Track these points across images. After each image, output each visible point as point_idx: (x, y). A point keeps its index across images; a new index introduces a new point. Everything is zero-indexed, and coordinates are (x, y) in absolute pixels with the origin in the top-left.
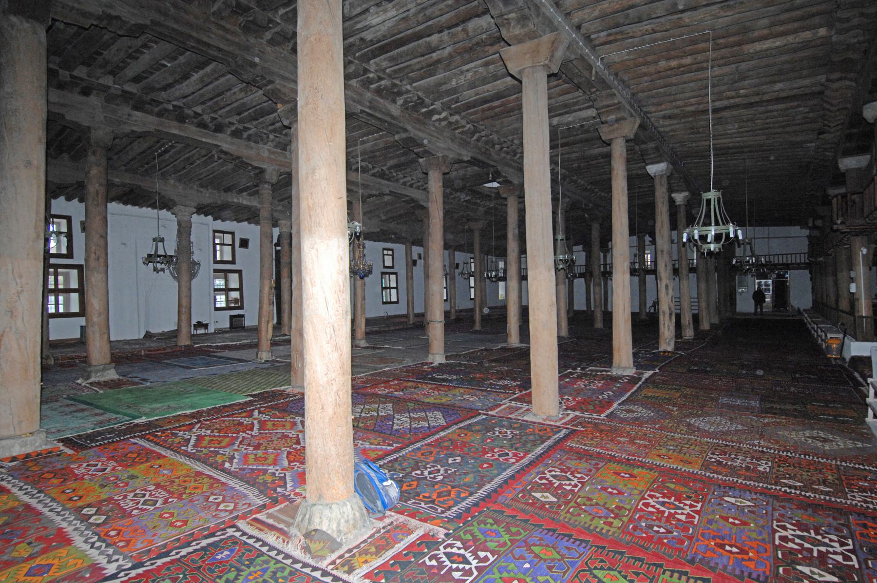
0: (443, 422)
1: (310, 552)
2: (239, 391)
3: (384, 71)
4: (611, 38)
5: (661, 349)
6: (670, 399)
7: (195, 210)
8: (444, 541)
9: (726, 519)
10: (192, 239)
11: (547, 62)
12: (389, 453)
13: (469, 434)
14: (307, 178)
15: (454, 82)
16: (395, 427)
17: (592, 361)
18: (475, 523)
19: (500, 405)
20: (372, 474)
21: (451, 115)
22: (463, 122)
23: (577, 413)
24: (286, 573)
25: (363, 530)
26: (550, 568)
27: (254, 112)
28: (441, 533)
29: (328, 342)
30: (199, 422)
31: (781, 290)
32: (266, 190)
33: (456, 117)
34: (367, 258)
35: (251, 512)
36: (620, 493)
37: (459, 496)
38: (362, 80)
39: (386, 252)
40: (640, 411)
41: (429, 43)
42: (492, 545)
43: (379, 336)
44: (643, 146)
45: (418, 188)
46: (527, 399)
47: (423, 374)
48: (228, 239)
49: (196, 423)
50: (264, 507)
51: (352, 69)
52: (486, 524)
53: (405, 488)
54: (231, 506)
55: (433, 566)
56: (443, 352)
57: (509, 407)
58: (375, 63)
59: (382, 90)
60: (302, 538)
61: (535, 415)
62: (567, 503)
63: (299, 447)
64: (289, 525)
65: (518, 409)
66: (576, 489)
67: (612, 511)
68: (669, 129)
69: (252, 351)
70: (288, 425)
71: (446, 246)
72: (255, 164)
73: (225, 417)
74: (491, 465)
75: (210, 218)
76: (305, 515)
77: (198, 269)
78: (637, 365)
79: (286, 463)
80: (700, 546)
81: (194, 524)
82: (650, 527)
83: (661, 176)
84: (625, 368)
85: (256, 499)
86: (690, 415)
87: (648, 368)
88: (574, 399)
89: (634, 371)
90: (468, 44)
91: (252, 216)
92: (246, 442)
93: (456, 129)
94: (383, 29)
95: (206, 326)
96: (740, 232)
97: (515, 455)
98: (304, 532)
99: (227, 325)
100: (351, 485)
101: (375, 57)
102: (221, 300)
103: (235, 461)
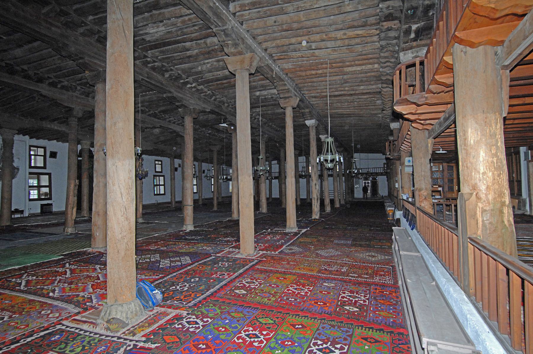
0: (190, 262)
1: (110, 330)
2: (54, 253)
3: (157, 57)
4: (282, 57)
5: (313, 218)
6: (312, 242)
7: (17, 132)
8: (186, 316)
9: (321, 292)
10: (14, 151)
11: (248, 68)
12: (157, 280)
13: (204, 266)
14: (111, 127)
15: (200, 68)
16: (161, 266)
17: (277, 225)
18: (203, 307)
19: (224, 251)
20: (147, 287)
21: (198, 85)
22: (206, 90)
23: (264, 252)
24: (96, 341)
25: (141, 317)
26: (238, 321)
27: (68, 72)
28: (185, 313)
29: (122, 216)
30: (26, 273)
31: (375, 185)
32: (73, 122)
33: (202, 87)
34: (144, 166)
35: (71, 316)
36: (278, 286)
37: (196, 296)
38: (143, 61)
39: (157, 162)
40: (296, 249)
41: (184, 46)
42: (211, 315)
43: (153, 215)
44: (303, 111)
45: (178, 124)
46: (238, 247)
47: (179, 237)
48: (41, 151)
49: (24, 274)
50: (79, 313)
51: (137, 54)
52: (209, 306)
53: (166, 295)
54: (57, 315)
55: (179, 328)
56: (192, 223)
57: (229, 252)
58: (152, 54)
59: (156, 68)
60: (105, 323)
61: (242, 254)
62: (251, 293)
63: (99, 281)
64: (96, 320)
65: (233, 252)
66: (257, 287)
67: (272, 294)
68: (315, 102)
69: (62, 228)
70: (91, 270)
71: (195, 159)
72: (66, 105)
73: (45, 268)
74: (215, 280)
75: (27, 137)
76: (106, 312)
77: (17, 172)
78: (300, 227)
79: (91, 290)
80: (307, 304)
81: (33, 325)
82: (288, 299)
83: (313, 126)
84: (292, 228)
85: (72, 309)
86: (317, 250)
87: (303, 228)
88: (264, 246)
89: (297, 229)
90: (207, 50)
91: (61, 137)
92: (62, 281)
93: (201, 93)
94: (157, 36)
95: (22, 212)
96: (342, 159)
97: (228, 274)
98: (106, 320)
99: (39, 211)
100: (134, 293)
101: (151, 49)
102: (34, 194)
103: (56, 292)
